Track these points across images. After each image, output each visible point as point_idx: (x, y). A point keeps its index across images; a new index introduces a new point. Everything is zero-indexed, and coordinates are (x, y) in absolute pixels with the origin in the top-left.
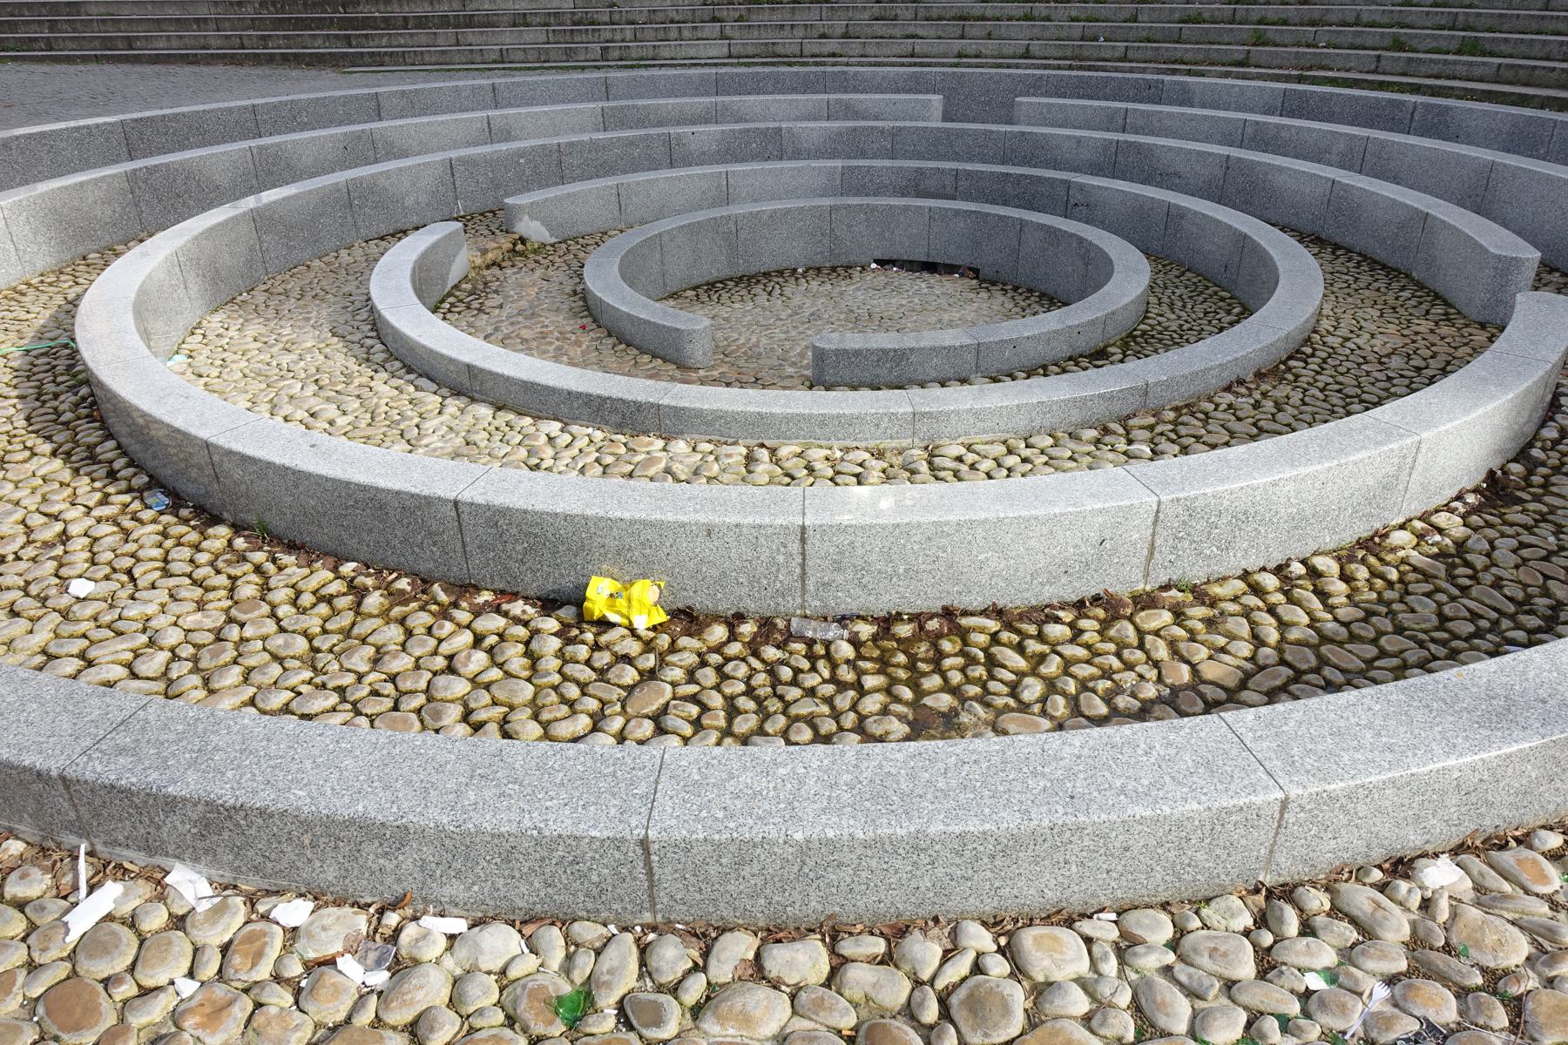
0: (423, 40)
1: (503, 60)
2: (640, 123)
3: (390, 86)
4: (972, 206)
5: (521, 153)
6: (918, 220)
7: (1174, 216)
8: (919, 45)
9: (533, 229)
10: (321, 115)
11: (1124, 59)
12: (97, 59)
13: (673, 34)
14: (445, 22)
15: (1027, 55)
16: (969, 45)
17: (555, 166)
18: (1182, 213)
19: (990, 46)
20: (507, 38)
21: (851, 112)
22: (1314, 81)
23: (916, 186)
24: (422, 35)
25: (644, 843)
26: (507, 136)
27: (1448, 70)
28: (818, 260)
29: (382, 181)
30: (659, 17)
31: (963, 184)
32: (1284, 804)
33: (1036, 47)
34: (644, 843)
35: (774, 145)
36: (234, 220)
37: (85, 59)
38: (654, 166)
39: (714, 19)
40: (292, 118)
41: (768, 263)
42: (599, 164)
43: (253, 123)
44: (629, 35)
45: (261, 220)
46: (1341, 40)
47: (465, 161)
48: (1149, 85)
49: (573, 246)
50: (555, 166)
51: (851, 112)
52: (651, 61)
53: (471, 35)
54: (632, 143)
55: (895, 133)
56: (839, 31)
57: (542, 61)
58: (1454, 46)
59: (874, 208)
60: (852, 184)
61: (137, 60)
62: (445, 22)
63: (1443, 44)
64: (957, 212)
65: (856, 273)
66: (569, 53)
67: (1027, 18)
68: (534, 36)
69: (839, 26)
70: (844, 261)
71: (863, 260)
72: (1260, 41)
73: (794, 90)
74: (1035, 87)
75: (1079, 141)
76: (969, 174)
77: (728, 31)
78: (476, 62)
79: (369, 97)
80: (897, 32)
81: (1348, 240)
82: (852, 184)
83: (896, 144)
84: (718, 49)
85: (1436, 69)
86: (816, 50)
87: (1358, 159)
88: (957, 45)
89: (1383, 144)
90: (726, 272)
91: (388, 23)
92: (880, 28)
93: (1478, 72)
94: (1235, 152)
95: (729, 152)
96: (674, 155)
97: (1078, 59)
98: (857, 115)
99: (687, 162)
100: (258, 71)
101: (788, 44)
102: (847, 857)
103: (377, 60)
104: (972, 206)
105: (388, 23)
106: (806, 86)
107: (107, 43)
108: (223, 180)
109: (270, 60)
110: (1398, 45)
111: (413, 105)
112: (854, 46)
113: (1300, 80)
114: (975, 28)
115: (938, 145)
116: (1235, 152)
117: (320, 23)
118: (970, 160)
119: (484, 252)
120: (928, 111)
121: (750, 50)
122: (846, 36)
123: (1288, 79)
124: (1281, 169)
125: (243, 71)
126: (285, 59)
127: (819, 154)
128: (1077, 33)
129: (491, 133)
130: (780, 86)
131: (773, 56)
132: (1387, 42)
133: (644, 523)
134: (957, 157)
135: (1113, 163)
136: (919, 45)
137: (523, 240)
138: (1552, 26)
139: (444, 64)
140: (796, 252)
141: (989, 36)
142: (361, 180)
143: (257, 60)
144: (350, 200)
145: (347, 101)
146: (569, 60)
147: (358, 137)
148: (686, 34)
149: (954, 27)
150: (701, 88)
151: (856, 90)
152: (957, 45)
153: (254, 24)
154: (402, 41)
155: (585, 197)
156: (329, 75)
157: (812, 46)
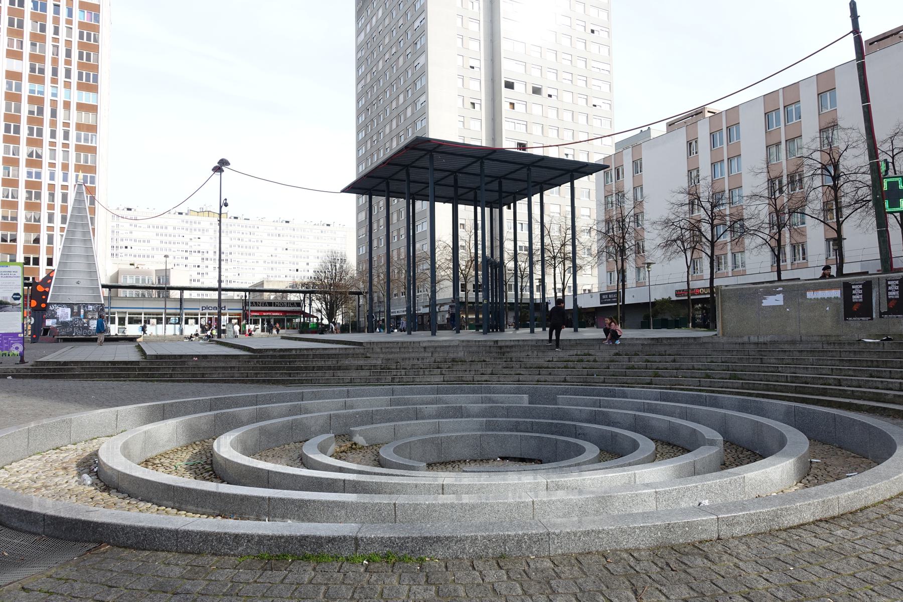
0: (320, 374)
1: (351, 382)
2: (405, 404)
3: (307, 390)
4: (538, 435)
5: (358, 413)
6: (515, 441)
7: (614, 436)
8: (521, 378)
9: (360, 440)
10: (280, 399)
11: (604, 382)
12: (190, 381)
13: (421, 373)
14: (329, 368)
15: (565, 381)
16: (542, 378)
17: (370, 418)
18: (617, 434)
19: (550, 378)
20: (354, 374)
21: (490, 400)
22: (675, 389)
23: (516, 427)
24: (320, 373)
25: (395, 504)
26: (352, 407)
27: (725, 385)
28: (475, 457)
29: (304, 420)
30: (416, 367)
31: (535, 427)
32: (533, 502)
33: (568, 378)
34: (395, 504)
35: (459, 412)
36: (254, 429)
37: (184, 381)
38: (410, 419)
39: (438, 368)
40: (270, 400)
41: (454, 457)
42: (387, 417)
43: (255, 401)
44: (403, 373)
45: (261, 429)
46: (687, 375)
47: (335, 415)
48: (610, 391)
49: (375, 445)
50: (370, 418)
51: (490, 400)
52: (413, 382)
53: (340, 373)
54: (401, 411)
55: (508, 409)
56: (489, 372)
57: (367, 382)
58: (728, 376)
59: (498, 436)
60: (489, 426)
61: (205, 381)
62: (329, 368)
63: (724, 376)
64: (531, 437)
65: (490, 462)
66: (378, 380)
67: (565, 367)
68: (365, 373)
69: (489, 371)
70: (486, 457)
71: (494, 457)
72: (657, 375)
73: (469, 393)
74: (565, 392)
75: (581, 410)
76: (537, 423)
77: (444, 372)
78: (340, 382)
79: (299, 393)
80: (512, 372)
81: (677, 443)
82: (489, 426)
83: (508, 412)
84: (439, 378)
85: (721, 385)
86: (479, 379)
87: (685, 415)
88: (537, 377)
89: (691, 409)
90: (436, 460)
91: (306, 368)
92: (506, 371)
93: (736, 385)
94: (638, 413)
95: (440, 415)
96: (418, 415)
97: (586, 383)
98: (494, 402)
99: (423, 418)
100: (253, 385)
101: (468, 377)
102: (437, 509)
103: (301, 382)
104: (538, 435)
105: (306, 368)
106: (474, 392)
107: (194, 375)
108: (245, 419)
109: (258, 382)
110: (708, 376)
111: (315, 396)
112: (495, 378)
113: (671, 389)
114: (543, 371)
115: (525, 412)
116: (638, 413)
117: (279, 368)
118: (539, 418)
119: (341, 447)
120: (524, 400)
121: (452, 379)
122: (492, 374)
123: (666, 389)
124: (653, 418)
125: (247, 385)
126: (264, 381)
127: (477, 416)
128: (585, 373)
129: (345, 406)
130: (463, 391)
131: (461, 381)
132: (704, 375)
133: (398, 484)
134: (534, 417)
135: (594, 418)
136: (521, 378)
137: (355, 444)
138: (770, 369)
139: (327, 383)
140: (466, 453)
141: (550, 374)
142: (297, 420)
143: (253, 382)
144: (292, 427)
145: (291, 394)
146: (378, 382)
147: (295, 406)
148: (426, 373)
149: (536, 371)
150: (431, 392)
151: (494, 393)
152: (537, 377)
153: (253, 368)
154: (312, 375)
155: (382, 429)
156: (281, 387)
157: (477, 378)
